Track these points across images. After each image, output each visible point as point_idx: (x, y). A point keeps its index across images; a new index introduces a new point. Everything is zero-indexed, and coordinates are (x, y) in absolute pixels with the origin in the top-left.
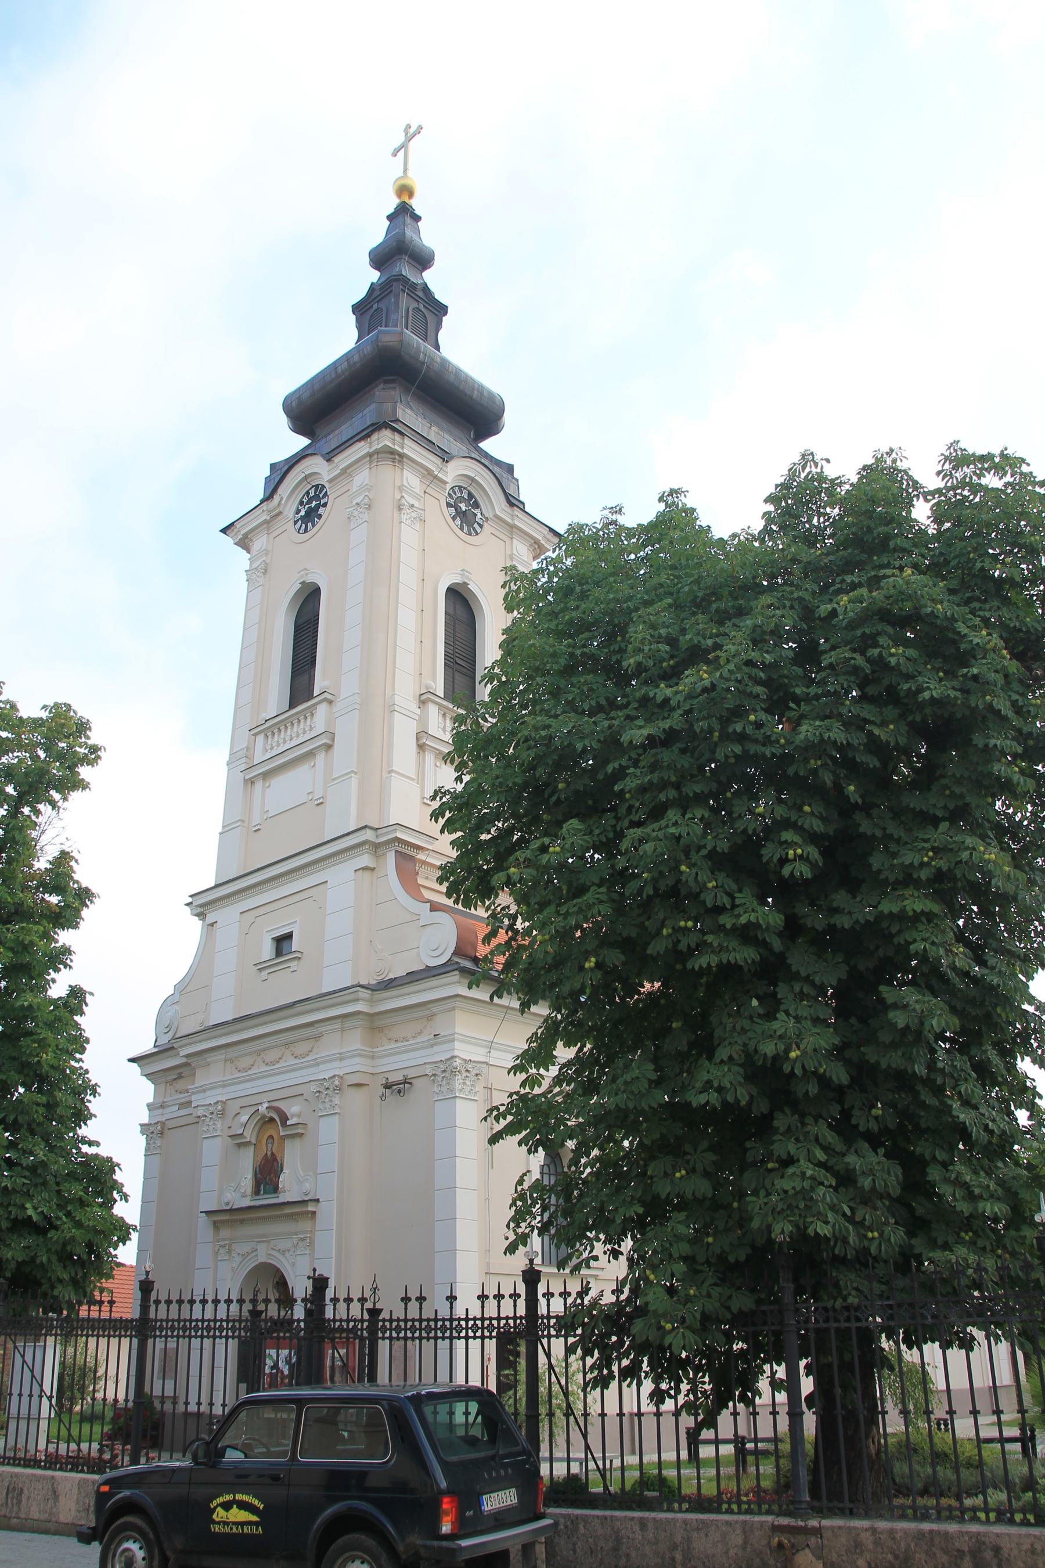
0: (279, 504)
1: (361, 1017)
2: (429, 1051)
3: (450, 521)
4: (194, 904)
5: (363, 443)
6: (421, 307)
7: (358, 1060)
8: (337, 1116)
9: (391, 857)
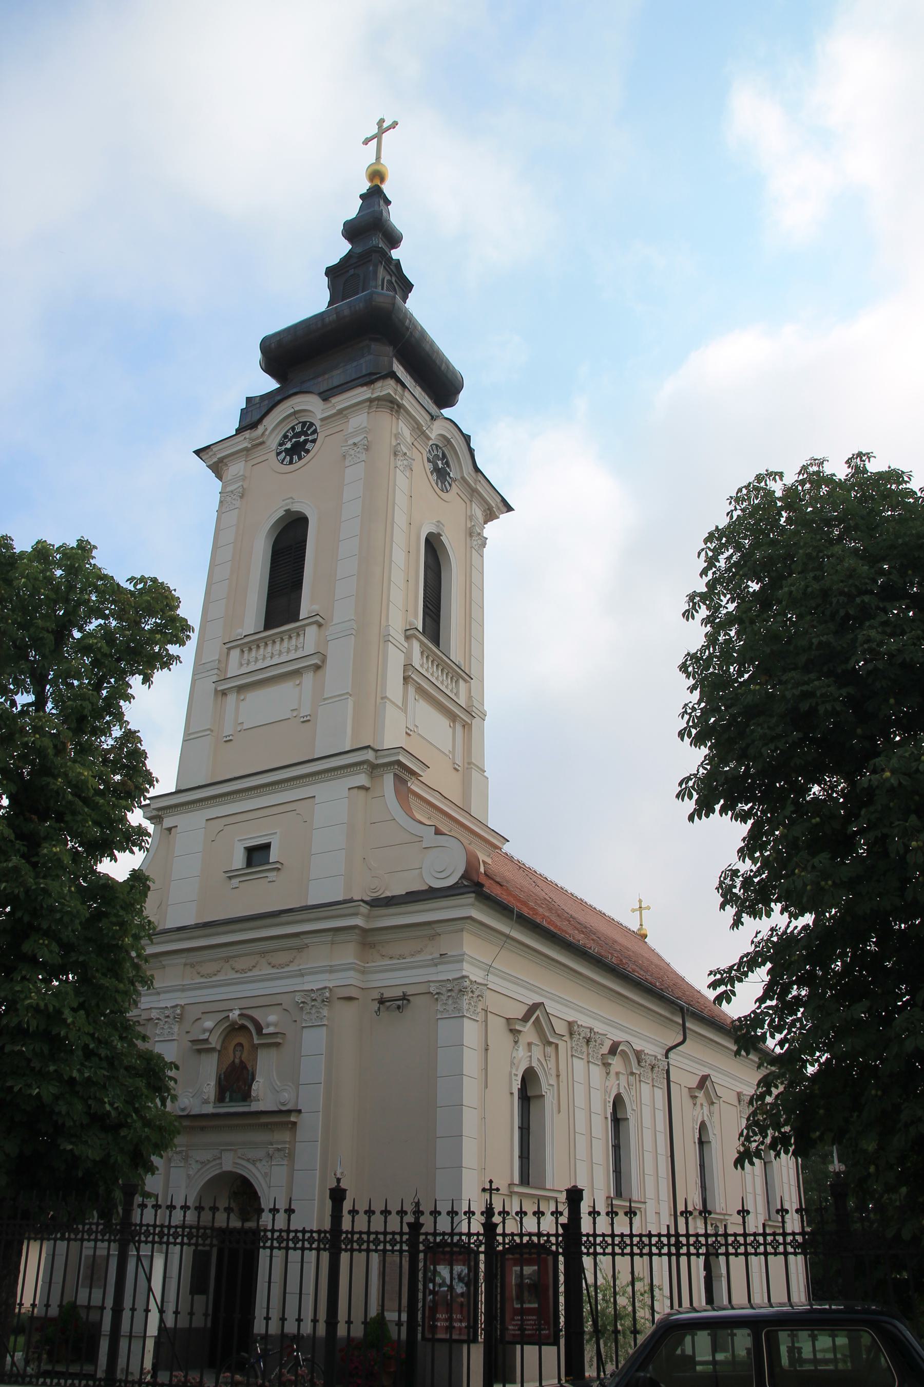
0: (263, 434)
1: (356, 931)
2: (433, 970)
3: (429, 474)
4: (152, 806)
5: (365, 388)
6: (393, 281)
7: (352, 973)
8: (325, 1028)
9: (388, 780)
